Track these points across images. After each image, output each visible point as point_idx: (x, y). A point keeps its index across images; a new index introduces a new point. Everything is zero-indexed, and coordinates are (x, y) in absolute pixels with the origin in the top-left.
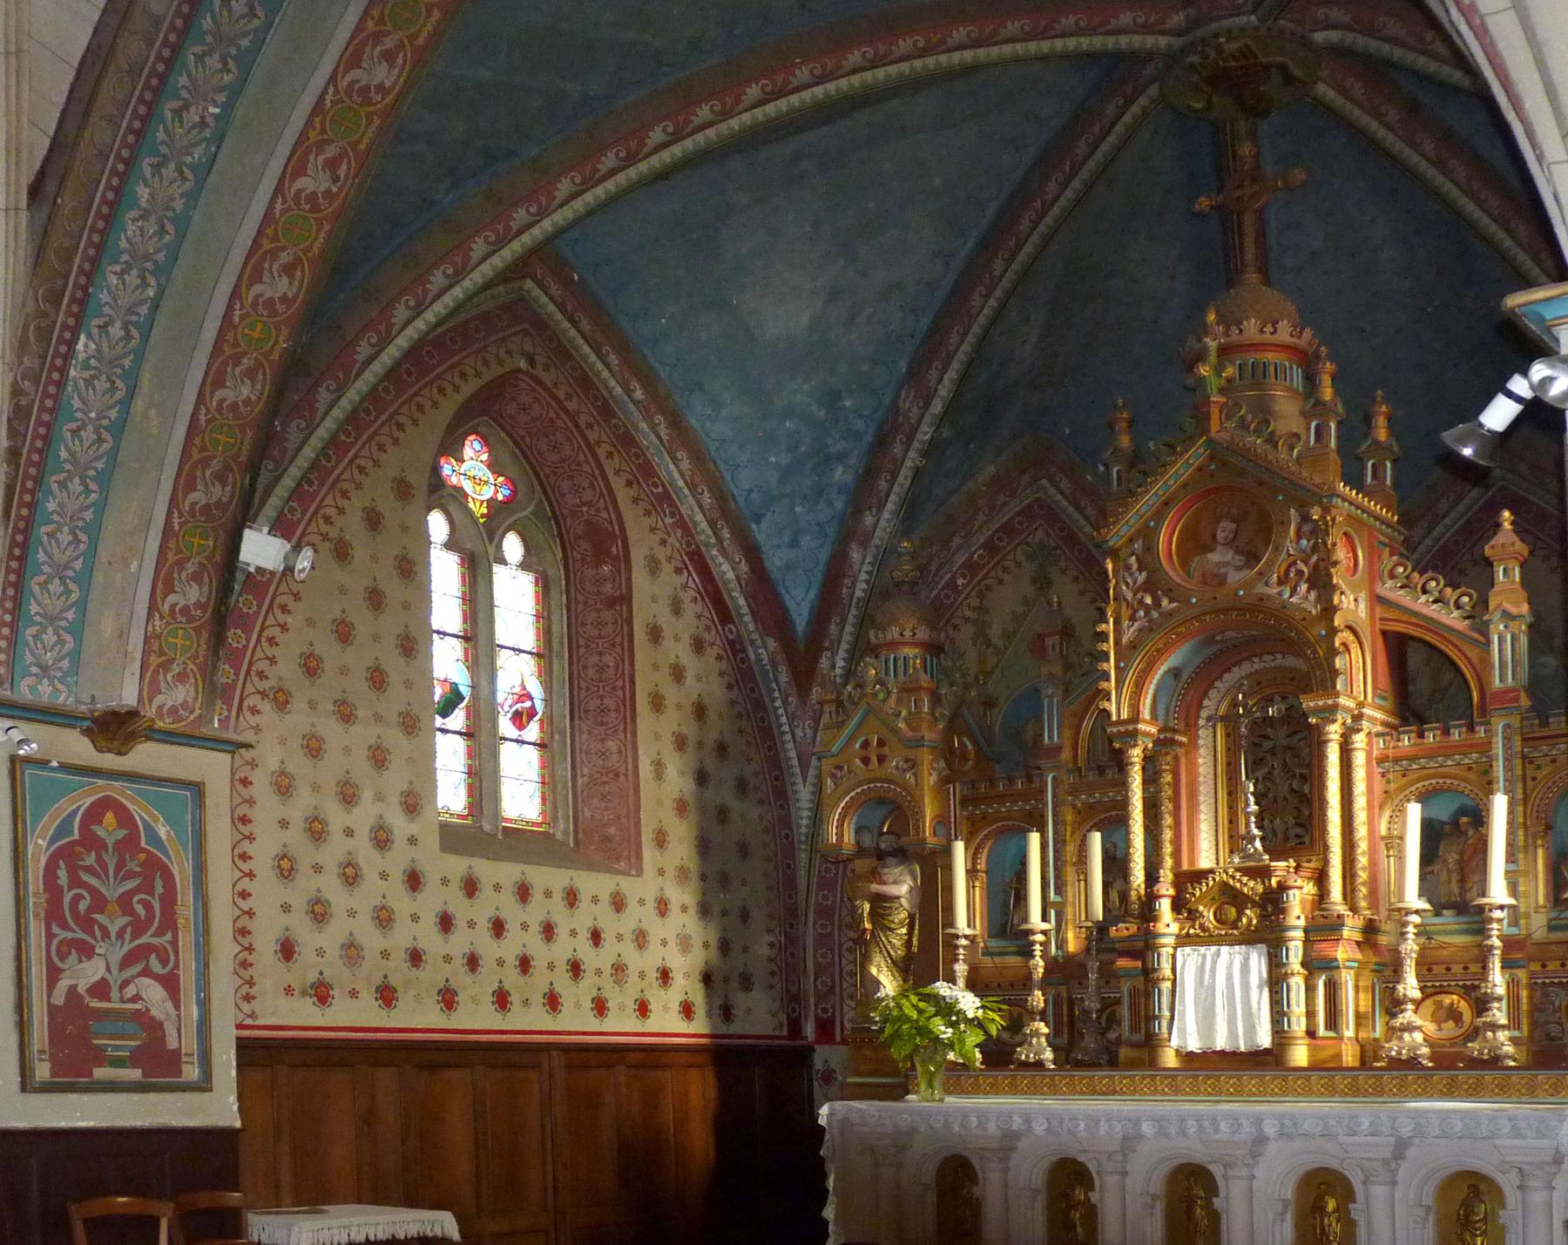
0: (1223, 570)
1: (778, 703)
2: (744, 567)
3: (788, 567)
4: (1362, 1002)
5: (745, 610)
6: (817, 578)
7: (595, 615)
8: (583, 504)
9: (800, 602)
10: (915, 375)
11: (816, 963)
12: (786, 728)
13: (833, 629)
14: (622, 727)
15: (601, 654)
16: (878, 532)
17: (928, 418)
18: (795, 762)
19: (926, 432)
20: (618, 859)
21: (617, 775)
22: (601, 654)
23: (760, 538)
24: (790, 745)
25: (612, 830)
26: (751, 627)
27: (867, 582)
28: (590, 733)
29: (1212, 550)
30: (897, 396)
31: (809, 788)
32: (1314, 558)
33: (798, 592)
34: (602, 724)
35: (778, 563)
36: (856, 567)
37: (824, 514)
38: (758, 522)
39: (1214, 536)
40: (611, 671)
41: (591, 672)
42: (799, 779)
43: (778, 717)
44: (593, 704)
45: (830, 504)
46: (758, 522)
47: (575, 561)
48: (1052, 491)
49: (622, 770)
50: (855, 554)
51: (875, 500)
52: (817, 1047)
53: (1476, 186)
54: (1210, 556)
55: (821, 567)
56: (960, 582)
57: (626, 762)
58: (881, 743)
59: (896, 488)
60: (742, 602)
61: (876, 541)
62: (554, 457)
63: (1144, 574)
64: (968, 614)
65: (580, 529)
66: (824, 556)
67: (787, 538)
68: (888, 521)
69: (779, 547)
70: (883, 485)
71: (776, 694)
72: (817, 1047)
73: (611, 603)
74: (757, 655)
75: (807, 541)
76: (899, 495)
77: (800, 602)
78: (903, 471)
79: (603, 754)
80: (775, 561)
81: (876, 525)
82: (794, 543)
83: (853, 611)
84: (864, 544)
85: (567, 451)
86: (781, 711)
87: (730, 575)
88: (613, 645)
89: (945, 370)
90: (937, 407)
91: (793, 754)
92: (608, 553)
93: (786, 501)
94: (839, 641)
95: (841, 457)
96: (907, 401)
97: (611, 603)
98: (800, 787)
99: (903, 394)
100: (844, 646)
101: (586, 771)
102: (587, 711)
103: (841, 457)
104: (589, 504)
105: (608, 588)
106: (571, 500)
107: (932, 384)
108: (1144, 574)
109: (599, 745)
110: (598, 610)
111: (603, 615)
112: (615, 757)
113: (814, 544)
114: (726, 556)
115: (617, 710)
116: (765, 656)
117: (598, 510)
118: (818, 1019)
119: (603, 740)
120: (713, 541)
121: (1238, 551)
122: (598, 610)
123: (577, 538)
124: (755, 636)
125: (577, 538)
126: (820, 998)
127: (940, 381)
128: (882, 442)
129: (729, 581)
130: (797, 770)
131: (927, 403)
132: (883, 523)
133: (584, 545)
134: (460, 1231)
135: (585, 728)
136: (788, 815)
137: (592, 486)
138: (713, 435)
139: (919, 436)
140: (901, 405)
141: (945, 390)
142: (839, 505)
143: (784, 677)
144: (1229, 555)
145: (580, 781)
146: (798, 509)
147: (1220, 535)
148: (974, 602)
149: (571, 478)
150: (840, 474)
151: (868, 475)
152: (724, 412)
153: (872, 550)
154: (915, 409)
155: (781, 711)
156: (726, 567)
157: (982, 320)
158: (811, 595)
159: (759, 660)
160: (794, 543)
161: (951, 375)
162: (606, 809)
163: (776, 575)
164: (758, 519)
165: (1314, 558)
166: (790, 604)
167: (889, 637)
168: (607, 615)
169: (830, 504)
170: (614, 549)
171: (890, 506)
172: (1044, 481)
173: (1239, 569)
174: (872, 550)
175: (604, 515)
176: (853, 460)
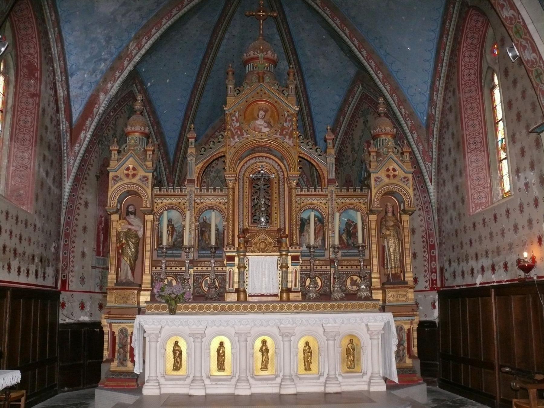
0: (260, 127)
1: (65, 148)
2: (66, 93)
3: (77, 96)
4: (290, 278)
5: (63, 109)
6: (84, 102)
7: (470, 105)
8: (29, 54)
9: (77, 110)
10: (138, 38)
11: (63, 256)
12: (66, 158)
13: (88, 123)
14: (31, 148)
15: (26, 116)
16: (112, 90)
17: (139, 55)
18: (66, 172)
19: (137, 59)
20: (23, 204)
21: (27, 168)
22: (26, 116)
23: (70, 83)
24: (66, 165)
25: (22, 192)
26: (63, 116)
27: (104, 107)
28: (18, 148)
29: (258, 120)
30: (129, 45)
31: (69, 184)
32: (291, 129)
33: (77, 106)
34: (23, 145)
35: (74, 94)
36: (101, 101)
37: (93, 79)
38: (71, 77)
39: (258, 116)
40: (29, 124)
41: (21, 122)
42: (66, 179)
43: (64, 153)
44: (21, 136)
45: (96, 76)
46: (71, 77)
47: (21, 76)
48: (136, 89)
49: (29, 166)
50: (102, 96)
51: (113, 79)
52: (62, 292)
53: (446, 32)
54: (257, 121)
55: (87, 99)
56: (111, 114)
57: (31, 163)
58: (134, 169)
59: (122, 76)
60: (63, 106)
61: (111, 93)
62: (24, 32)
63: (239, 123)
64: (112, 126)
65: (25, 63)
66: (89, 94)
67: (79, 85)
68: (116, 87)
69: (76, 87)
70: (117, 74)
71: (65, 144)
72: (62, 292)
73: (33, 95)
74: (63, 127)
75: (85, 88)
76: (122, 78)
77: (77, 110)
78: (126, 71)
79: (23, 158)
80: (73, 93)
81: (112, 87)
82: (81, 88)
83: (97, 117)
84: (106, 93)
85: (30, 31)
86: (65, 151)
87: (62, 95)
88: (31, 113)
89: (148, 39)
90: (143, 51)
91: (66, 169)
92: (34, 75)
93: (83, 71)
94: (90, 127)
95: (105, 60)
96: (132, 46)
97: (33, 95)
98: (66, 183)
99: (131, 44)
100: (91, 130)
101: (14, 164)
102: (18, 139)
103: (105, 60)
104: (31, 55)
105: (32, 89)
106: (25, 51)
107: (143, 43)
108: (239, 123)
109: (21, 154)
110: (27, 98)
111: (29, 100)
112: (27, 160)
113: (87, 90)
114: (62, 87)
115: (30, 140)
116: (65, 128)
117: (34, 58)
118: (62, 280)
119: (23, 152)
120: (60, 80)
121: (265, 122)
122: (27, 98)
123: (23, 66)
124: (64, 120)
125: (23, 66)
126: (63, 270)
127: (146, 43)
128: (120, 58)
129: (60, 97)
130: (66, 176)
131: (140, 49)
132: (114, 87)
133: (25, 70)
134: (399, 379)
135: (16, 146)
136: (61, 193)
137: (34, 48)
138: (68, 41)
139: (135, 60)
140: (130, 47)
141: (147, 46)
142: (99, 77)
143: (68, 138)
144: (262, 123)
145: (11, 168)
146: (86, 76)
147: (260, 116)
148: (114, 122)
149: (28, 42)
150: (102, 66)
151: (112, 69)
152: (74, 33)
153: (108, 96)
154: (135, 50)
155: (65, 151)
156: (61, 91)
157: (165, 27)
158: (81, 108)
159: (63, 129)
160: (81, 88)
161: (150, 42)
162: (21, 182)
163: (72, 98)
164: (72, 75)
165: (291, 129)
166: (73, 110)
167: (136, 129)
168: (30, 100)
169: (96, 76)
170: (36, 75)
171: (118, 82)
172: (134, 85)
173: (266, 127)
174: (108, 96)
175: (36, 60)
176: (108, 62)
